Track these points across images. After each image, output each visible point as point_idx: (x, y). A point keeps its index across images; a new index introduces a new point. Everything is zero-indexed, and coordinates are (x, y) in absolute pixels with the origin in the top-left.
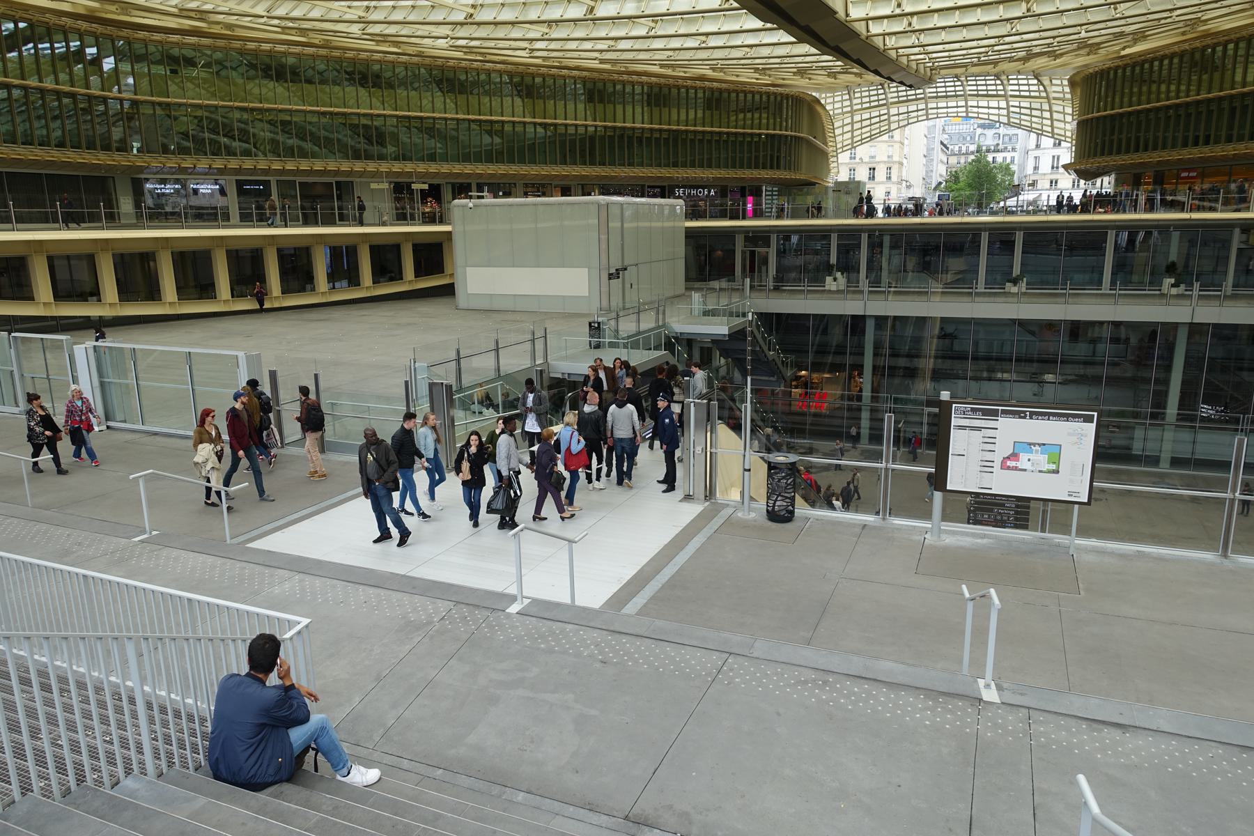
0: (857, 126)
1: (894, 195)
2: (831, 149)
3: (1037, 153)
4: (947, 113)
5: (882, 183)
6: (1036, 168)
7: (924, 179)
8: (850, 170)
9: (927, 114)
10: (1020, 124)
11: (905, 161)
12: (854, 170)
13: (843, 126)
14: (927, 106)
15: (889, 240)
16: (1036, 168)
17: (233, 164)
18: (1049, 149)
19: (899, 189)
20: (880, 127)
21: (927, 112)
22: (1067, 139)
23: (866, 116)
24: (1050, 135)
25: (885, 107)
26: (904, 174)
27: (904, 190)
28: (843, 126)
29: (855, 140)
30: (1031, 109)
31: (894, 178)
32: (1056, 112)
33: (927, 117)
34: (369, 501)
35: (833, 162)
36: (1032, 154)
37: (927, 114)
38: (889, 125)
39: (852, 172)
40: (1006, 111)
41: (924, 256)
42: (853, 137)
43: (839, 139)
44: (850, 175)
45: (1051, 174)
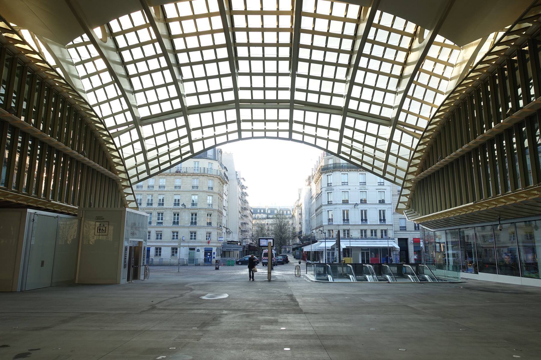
1: (214, 237)
3: (330, 207)
5: (203, 227)
7: (240, 228)
8: (175, 215)
9: (239, 131)
11: (224, 212)
12: (178, 215)
17: (187, 244)
18: (339, 204)
22: (398, 180)
24: (381, 173)
32: (383, 151)
33: (240, 135)
37: (239, 131)
40: (338, 134)
41: (242, 189)
43: (130, 163)
44: (192, 219)
45: (343, 225)
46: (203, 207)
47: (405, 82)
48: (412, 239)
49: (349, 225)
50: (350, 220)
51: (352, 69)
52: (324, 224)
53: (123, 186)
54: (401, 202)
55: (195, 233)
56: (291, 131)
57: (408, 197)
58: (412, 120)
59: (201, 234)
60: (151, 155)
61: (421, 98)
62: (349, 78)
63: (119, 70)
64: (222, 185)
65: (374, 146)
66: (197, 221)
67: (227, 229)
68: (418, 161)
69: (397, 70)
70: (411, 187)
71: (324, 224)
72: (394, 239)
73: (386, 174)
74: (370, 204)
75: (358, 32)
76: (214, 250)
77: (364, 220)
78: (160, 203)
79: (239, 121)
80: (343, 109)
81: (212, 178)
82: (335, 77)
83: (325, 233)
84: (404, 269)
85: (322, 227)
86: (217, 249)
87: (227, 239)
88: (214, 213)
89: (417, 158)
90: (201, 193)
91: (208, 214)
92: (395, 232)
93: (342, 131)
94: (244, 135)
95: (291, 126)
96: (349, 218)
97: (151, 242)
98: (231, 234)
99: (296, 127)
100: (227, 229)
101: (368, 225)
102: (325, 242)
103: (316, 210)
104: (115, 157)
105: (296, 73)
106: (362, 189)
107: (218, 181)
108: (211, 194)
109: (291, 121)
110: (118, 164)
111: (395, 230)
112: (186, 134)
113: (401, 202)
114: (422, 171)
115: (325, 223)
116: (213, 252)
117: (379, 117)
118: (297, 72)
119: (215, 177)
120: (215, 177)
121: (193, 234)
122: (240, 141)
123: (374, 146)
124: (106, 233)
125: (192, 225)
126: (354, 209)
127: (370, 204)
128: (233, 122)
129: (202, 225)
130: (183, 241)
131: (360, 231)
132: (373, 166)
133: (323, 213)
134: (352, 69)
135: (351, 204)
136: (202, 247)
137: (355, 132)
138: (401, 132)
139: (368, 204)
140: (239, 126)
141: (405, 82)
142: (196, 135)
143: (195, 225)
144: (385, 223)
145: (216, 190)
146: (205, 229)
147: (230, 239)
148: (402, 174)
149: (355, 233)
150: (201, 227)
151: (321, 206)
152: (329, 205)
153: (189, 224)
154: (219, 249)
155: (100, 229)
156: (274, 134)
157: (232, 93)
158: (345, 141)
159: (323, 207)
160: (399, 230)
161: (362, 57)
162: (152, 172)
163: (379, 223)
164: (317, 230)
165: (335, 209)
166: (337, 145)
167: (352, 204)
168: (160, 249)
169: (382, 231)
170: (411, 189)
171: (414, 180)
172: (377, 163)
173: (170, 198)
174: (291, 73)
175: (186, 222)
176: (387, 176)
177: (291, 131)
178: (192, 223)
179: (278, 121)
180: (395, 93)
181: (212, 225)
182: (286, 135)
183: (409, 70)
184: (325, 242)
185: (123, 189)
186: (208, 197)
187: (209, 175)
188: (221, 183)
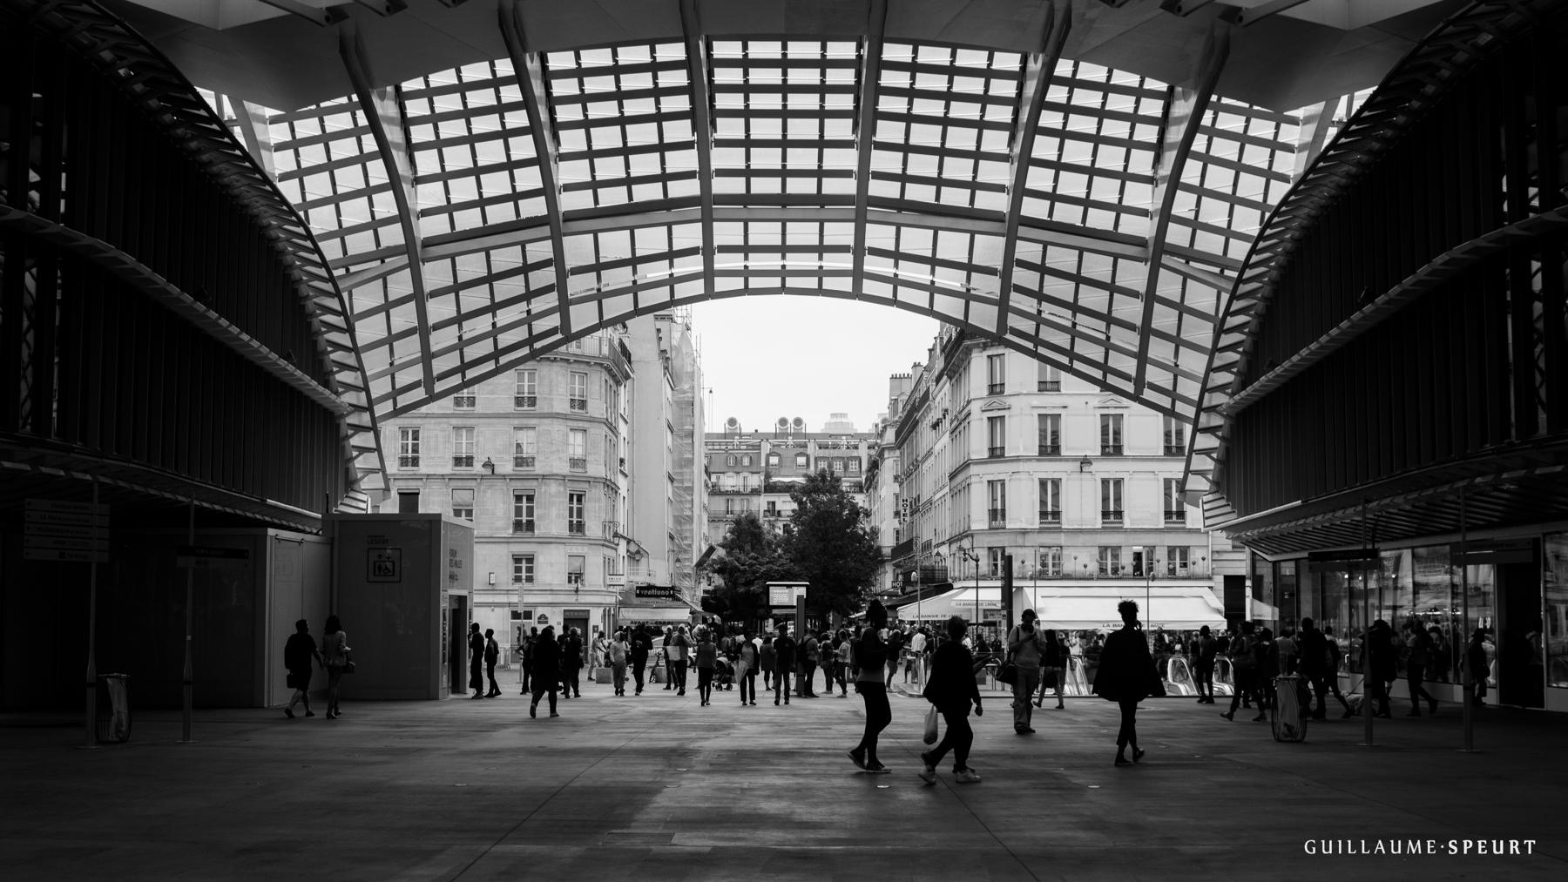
0: (440, 309)
1: (594, 576)
2: (349, 398)
3: (996, 471)
4: (783, 273)
6: (997, 514)
7: (672, 537)
8: (518, 498)
9: (709, 274)
10: (1035, 339)
12: (530, 499)
13: (387, 307)
14: (708, 234)
15: (1226, 99)
16: (997, 514)
17: (503, 599)
18: (1029, 459)
19: (609, 563)
20: (530, 318)
21: (709, 262)
22: (1181, 408)
23: (472, 267)
24: (1129, 387)
25: (546, 231)
26: (621, 518)
27: (622, 566)
28: (387, 307)
29: (439, 366)
30: (1078, 279)
31: (593, 528)
32: (1131, 327)
33: (709, 285)
34: (1139, 337)
35: (363, 450)
36: (979, 478)
38: (564, 307)
39: (524, 504)
42: (427, 357)
43: (375, 362)
44: (518, 511)
45: (1041, 531)
46: (555, 472)
47: (1170, 157)
48: (1262, 573)
49: (1060, 530)
50: (1064, 517)
51: (1020, 135)
52: (974, 527)
53: (350, 425)
54: (1197, 473)
55: (530, 560)
56: (858, 274)
57: (1215, 455)
58: (1210, 243)
59: (551, 565)
60: (442, 339)
61: (1229, 191)
62: (1017, 150)
63: (393, 134)
64: (614, 388)
65: (1106, 312)
66: (535, 518)
67: (629, 541)
68: (1233, 357)
69: (1148, 134)
70: (1221, 426)
71: (974, 527)
72: (1210, 578)
73: (866, 282)
74: (1135, 459)
75: (1024, 91)
76: (596, 618)
77: (1112, 513)
78: (407, 458)
79: (708, 250)
80: (1007, 217)
81: (582, 366)
82: (978, 146)
83: (977, 561)
84: (1014, 645)
85: (967, 536)
86: (604, 615)
87: (632, 578)
88: (593, 490)
89: (1232, 347)
90: (546, 421)
91: (571, 496)
92: (1216, 556)
93: (1006, 275)
94: (721, 284)
95: (859, 262)
96: (1063, 507)
97: (599, 605)
98: (644, 561)
99: (872, 264)
100: (629, 541)
101: (1126, 531)
102: (977, 587)
103: (952, 476)
104: (338, 347)
105: (874, 139)
106: (1108, 404)
107: (605, 375)
108: (581, 424)
109: (859, 250)
110: (344, 367)
111: (1217, 548)
112: (553, 280)
113: (1197, 473)
114: (1243, 386)
115: (980, 522)
116: (592, 623)
117: (1111, 236)
118: (875, 136)
119: (593, 362)
120: (593, 362)
121: (524, 565)
122: (710, 302)
123: (1106, 312)
124: (397, 579)
125: (519, 533)
126: (1077, 476)
127: (1135, 459)
128: (692, 251)
129: (555, 531)
130: (490, 587)
131: (1096, 551)
132: (1104, 367)
133: (972, 487)
134: (1020, 135)
135: (1067, 459)
136: (554, 609)
137: (1047, 277)
138: (1182, 277)
139: (1127, 458)
140: (709, 262)
141: (1170, 157)
142: (578, 285)
143: (530, 533)
144: (1184, 523)
145: (596, 408)
146: (561, 547)
147: (642, 579)
148: (1191, 389)
149: (1081, 558)
150: (547, 541)
151: (966, 465)
152: (992, 462)
153: (508, 529)
154: (609, 616)
155: (380, 568)
156: (812, 283)
157: (718, 240)
158: (1016, 300)
159: (973, 469)
160: (1230, 548)
161: (1051, 86)
162: (439, 387)
163: (1162, 525)
164: (954, 547)
165: (1015, 476)
166: (994, 311)
167: (1074, 459)
168: (1168, 450)
169: (1171, 551)
170: (1220, 434)
171: (1230, 407)
172: (1117, 361)
173: (441, 440)
174: (858, 140)
175: (500, 524)
176: (1148, 394)
177: (858, 274)
178: (518, 525)
179: (821, 249)
180: (1150, 180)
181: (587, 533)
182: (846, 284)
183: (1176, 134)
184: (977, 587)
185: (348, 437)
186: (571, 435)
187: (572, 359)
188: (611, 382)
